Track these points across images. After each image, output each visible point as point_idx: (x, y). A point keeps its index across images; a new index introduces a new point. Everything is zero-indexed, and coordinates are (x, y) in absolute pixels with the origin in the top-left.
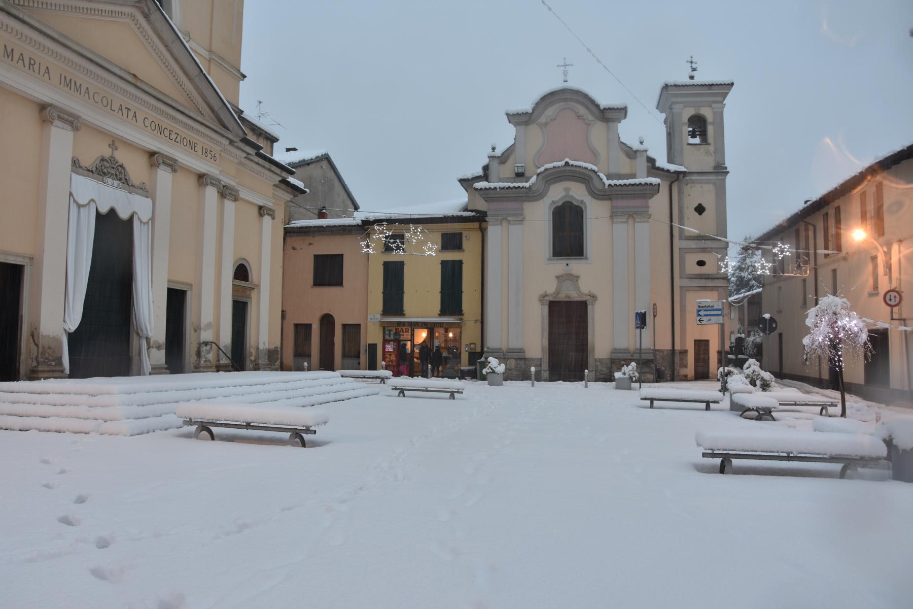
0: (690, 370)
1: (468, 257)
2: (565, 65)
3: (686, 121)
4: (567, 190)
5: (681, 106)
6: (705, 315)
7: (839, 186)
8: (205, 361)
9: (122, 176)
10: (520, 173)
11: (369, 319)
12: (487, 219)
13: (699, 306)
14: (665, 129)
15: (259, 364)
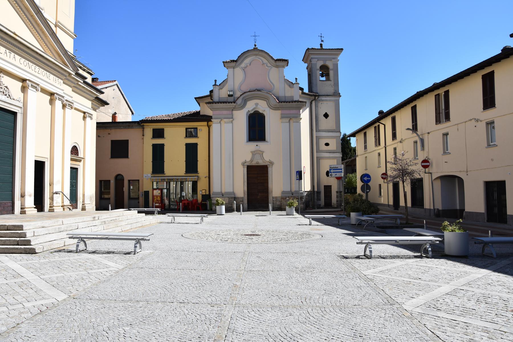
0: (322, 202)
1: (201, 141)
2: (255, 36)
3: (319, 68)
4: (257, 104)
5: (316, 60)
6: (333, 172)
8: (56, 203)
9: (7, 93)
10: (230, 95)
11: (144, 177)
14: (307, 72)
15: (53, 206)
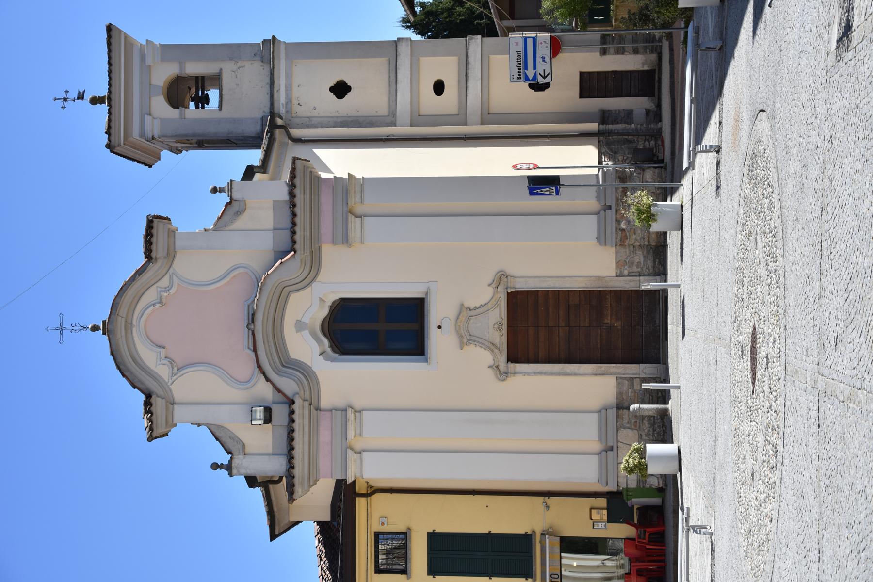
0: (638, 104)
3: (177, 110)
4: (300, 326)
6: (535, 67)
7: (260, 477)
12: (349, 481)
13: (518, 78)
14: (192, 153)
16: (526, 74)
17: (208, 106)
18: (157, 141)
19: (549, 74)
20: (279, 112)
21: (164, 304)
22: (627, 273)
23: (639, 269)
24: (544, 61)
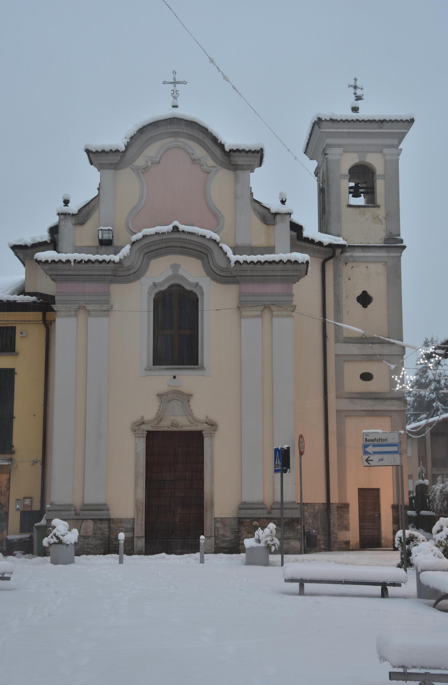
3: (347, 172)
4: (175, 267)
6: (374, 453)
13: (366, 439)
16: (370, 445)
17: (351, 196)
18: (324, 157)
19: (369, 464)
20: (347, 252)
21: (194, 161)
22: (218, 526)
23: (220, 537)
24: (380, 460)
